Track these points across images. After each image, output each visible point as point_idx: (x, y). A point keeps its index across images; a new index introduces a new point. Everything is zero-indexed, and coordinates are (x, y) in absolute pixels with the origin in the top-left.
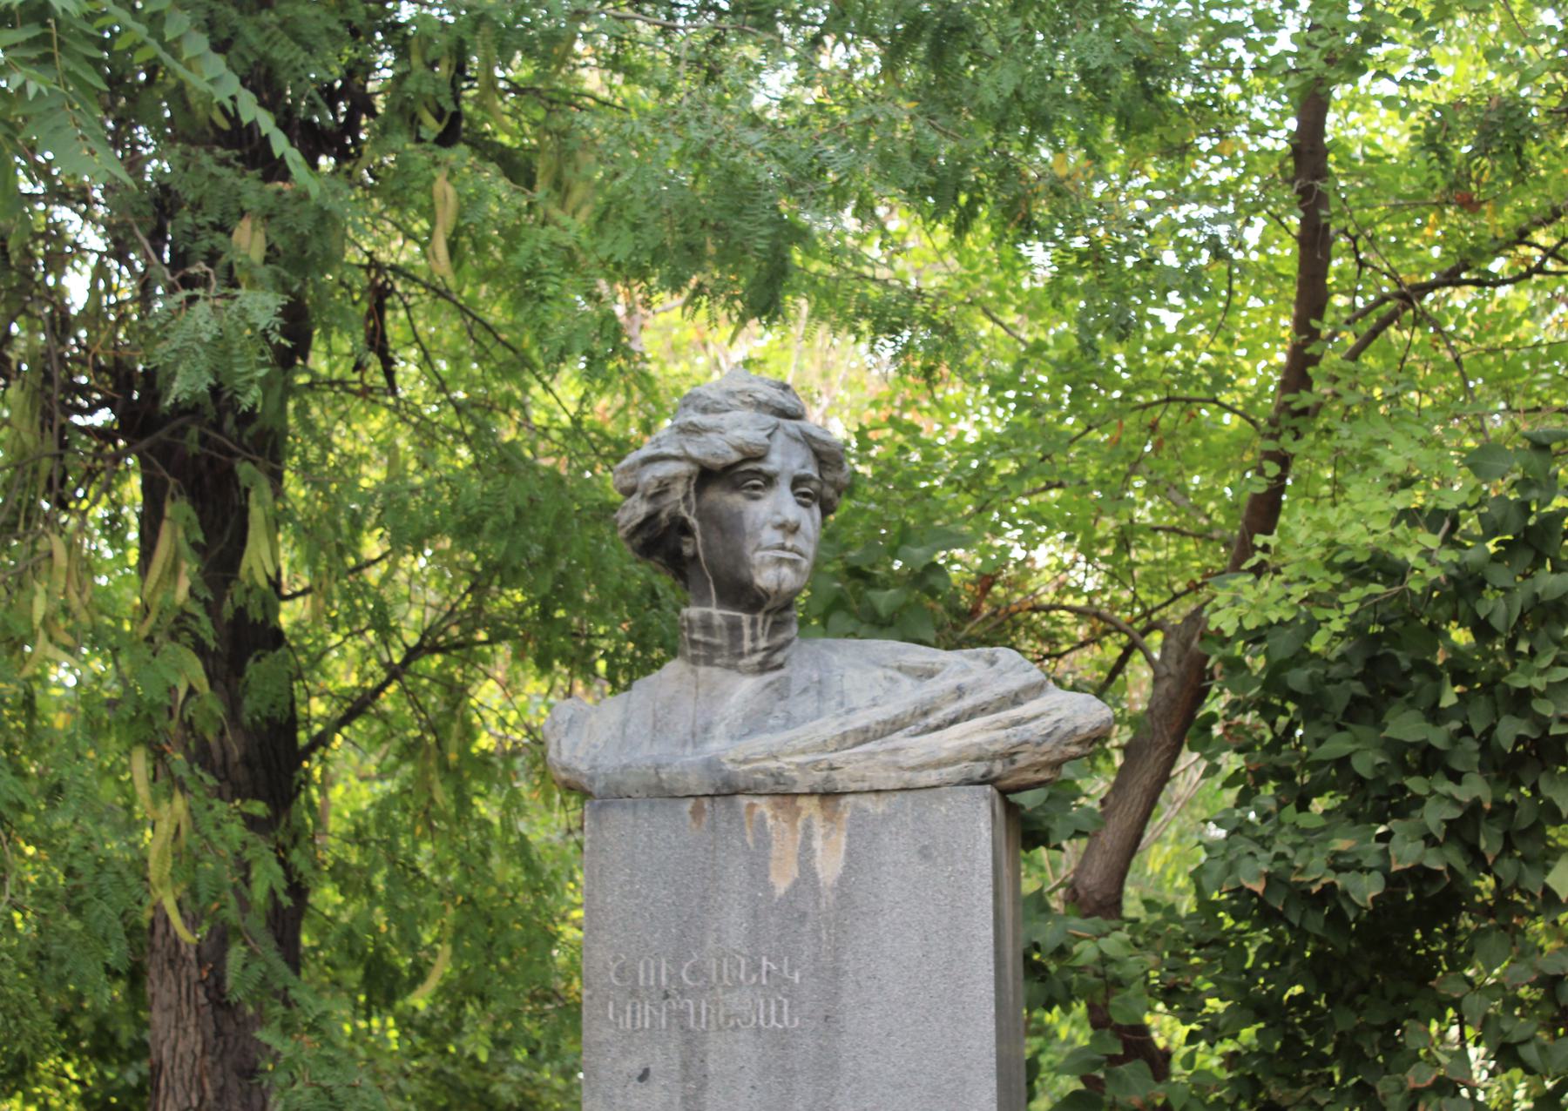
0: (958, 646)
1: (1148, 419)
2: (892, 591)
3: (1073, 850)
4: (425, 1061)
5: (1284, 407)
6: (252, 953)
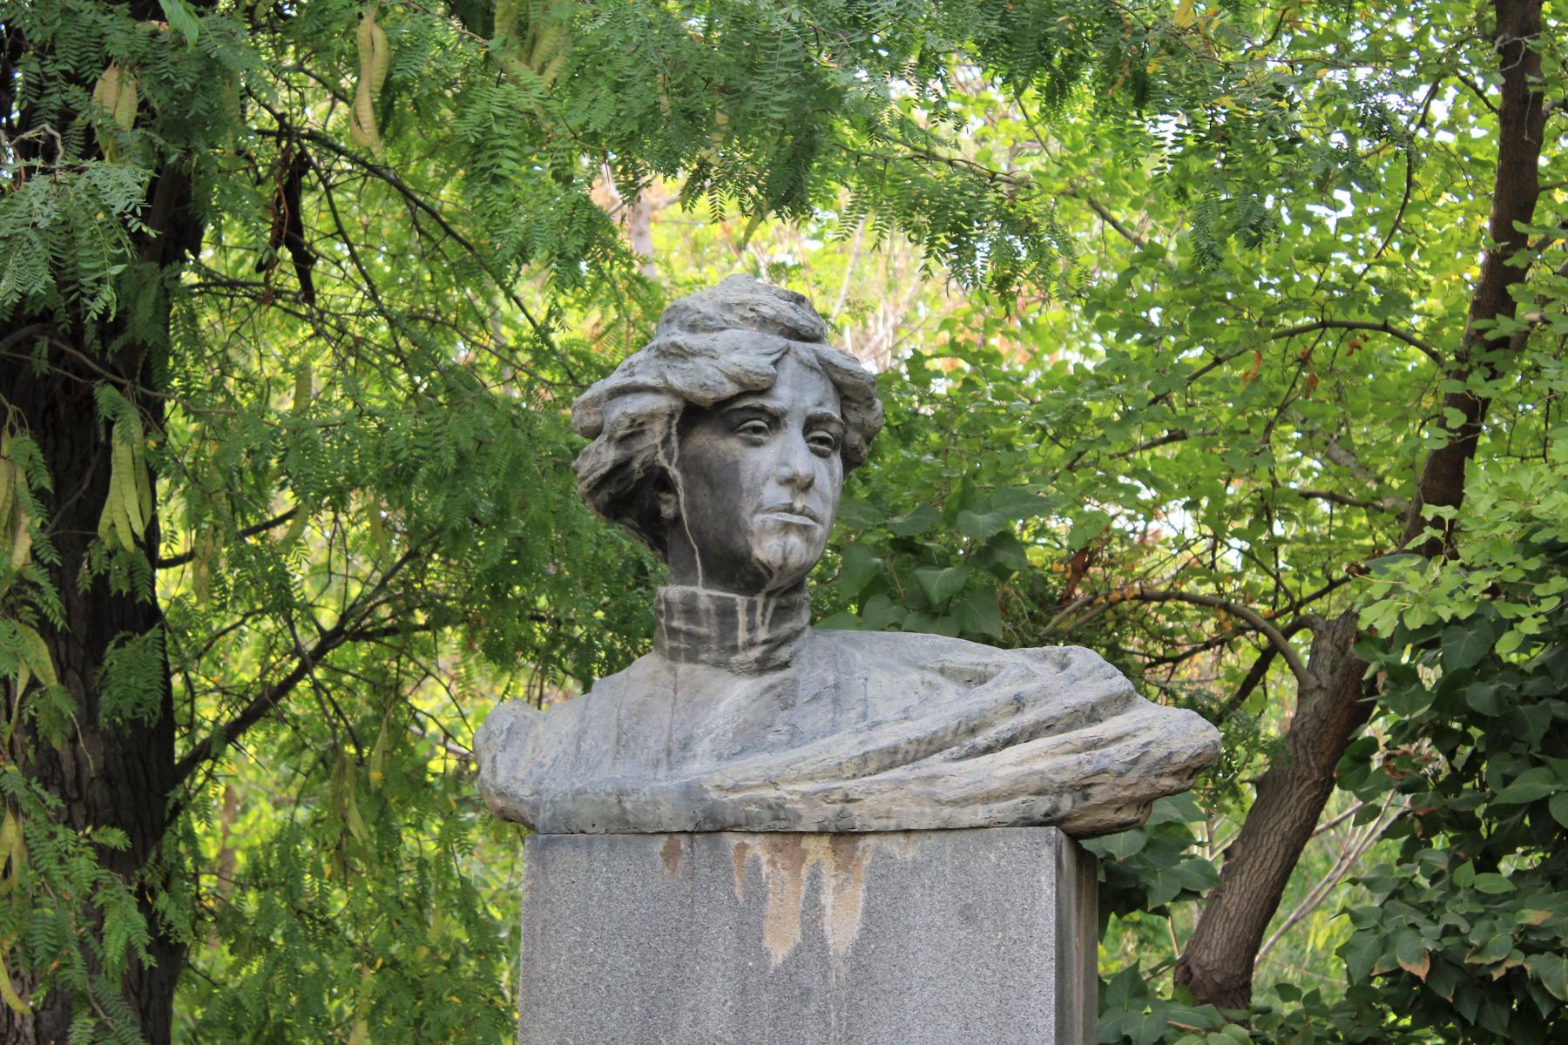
1: (1297, 349)
3: (1188, 915)
5: (1475, 337)
6: (102, 1028)
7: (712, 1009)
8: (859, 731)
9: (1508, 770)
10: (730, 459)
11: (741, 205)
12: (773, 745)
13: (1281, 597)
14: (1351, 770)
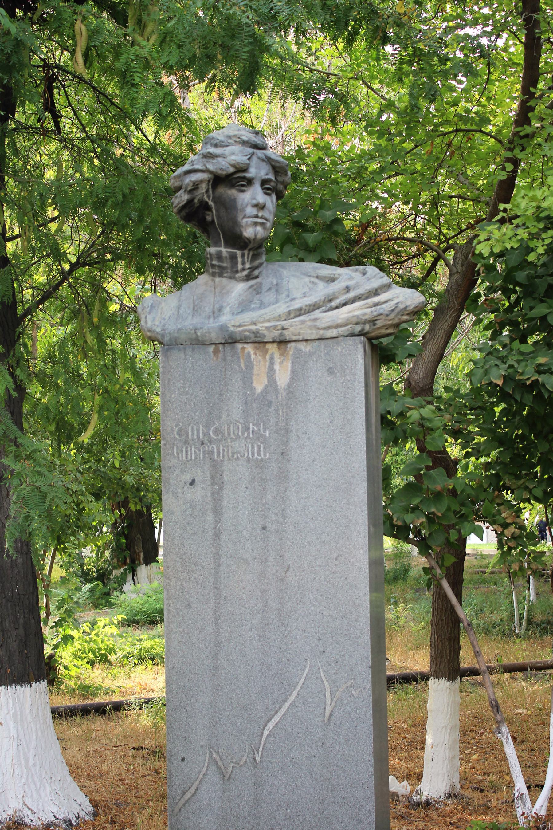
0: (348, 264)
1: (447, 140)
4: (90, 465)
5: (516, 134)
7: (234, 410)
8: (286, 302)
9: (532, 305)
10: (232, 197)
13: (442, 237)
14: (471, 305)
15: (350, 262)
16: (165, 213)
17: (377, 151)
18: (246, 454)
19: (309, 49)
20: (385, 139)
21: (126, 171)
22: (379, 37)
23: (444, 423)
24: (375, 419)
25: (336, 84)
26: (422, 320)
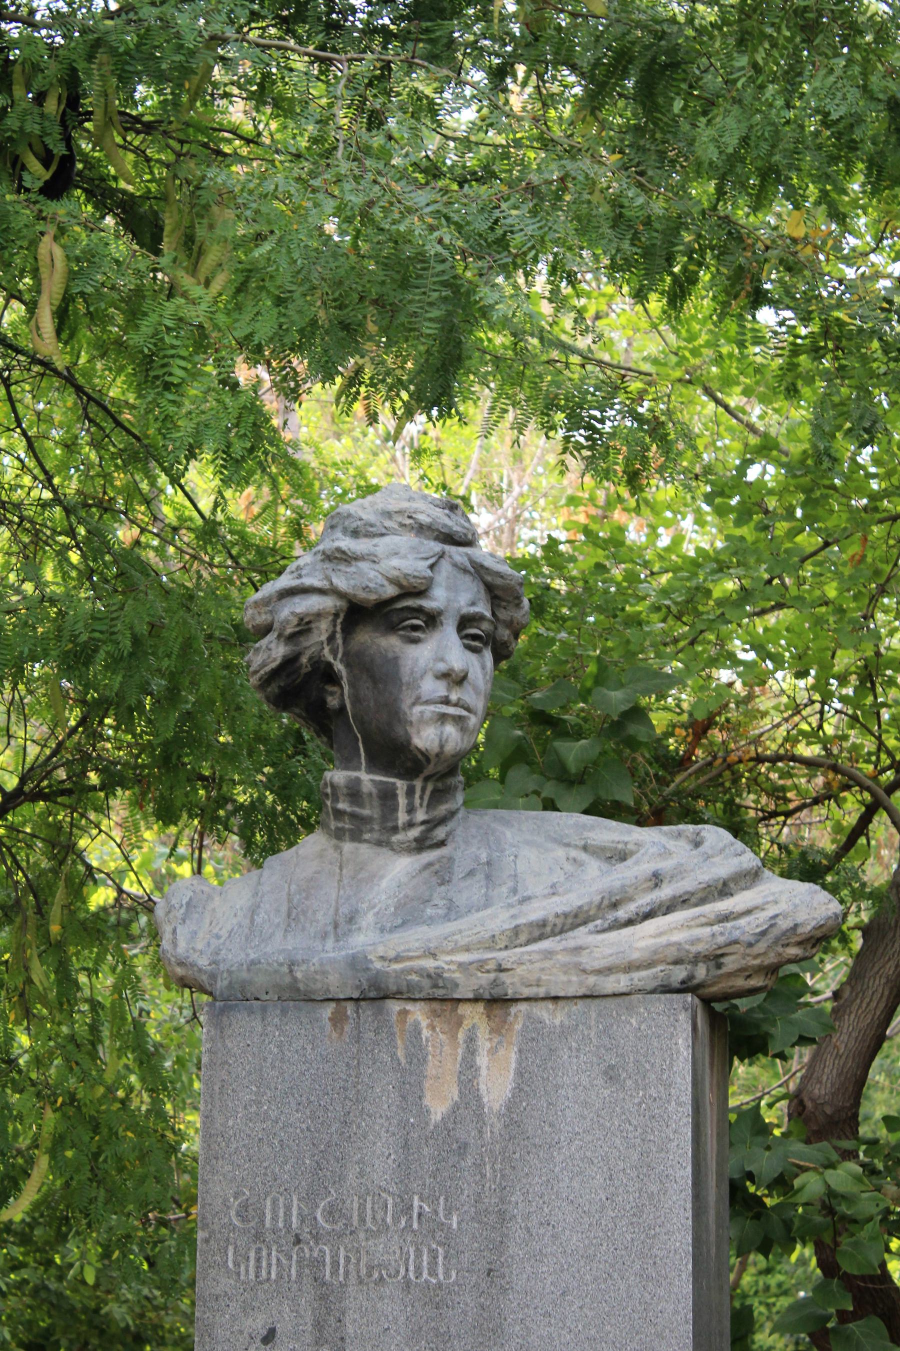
0: (657, 817)
2: (583, 742)
4: (25, 1274)
8: (511, 906)
10: (390, 655)
11: (394, 409)
12: (431, 918)
13: (883, 756)
15: (663, 810)
16: (233, 683)
17: (735, 553)
18: (402, 1271)
19: (580, 313)
20: (752, 524)
21: (142, 583)
22: (743, 293)
23: (882, 1206)
24: (715, 1193)
25: (640, 397)
26: (834, 951)
